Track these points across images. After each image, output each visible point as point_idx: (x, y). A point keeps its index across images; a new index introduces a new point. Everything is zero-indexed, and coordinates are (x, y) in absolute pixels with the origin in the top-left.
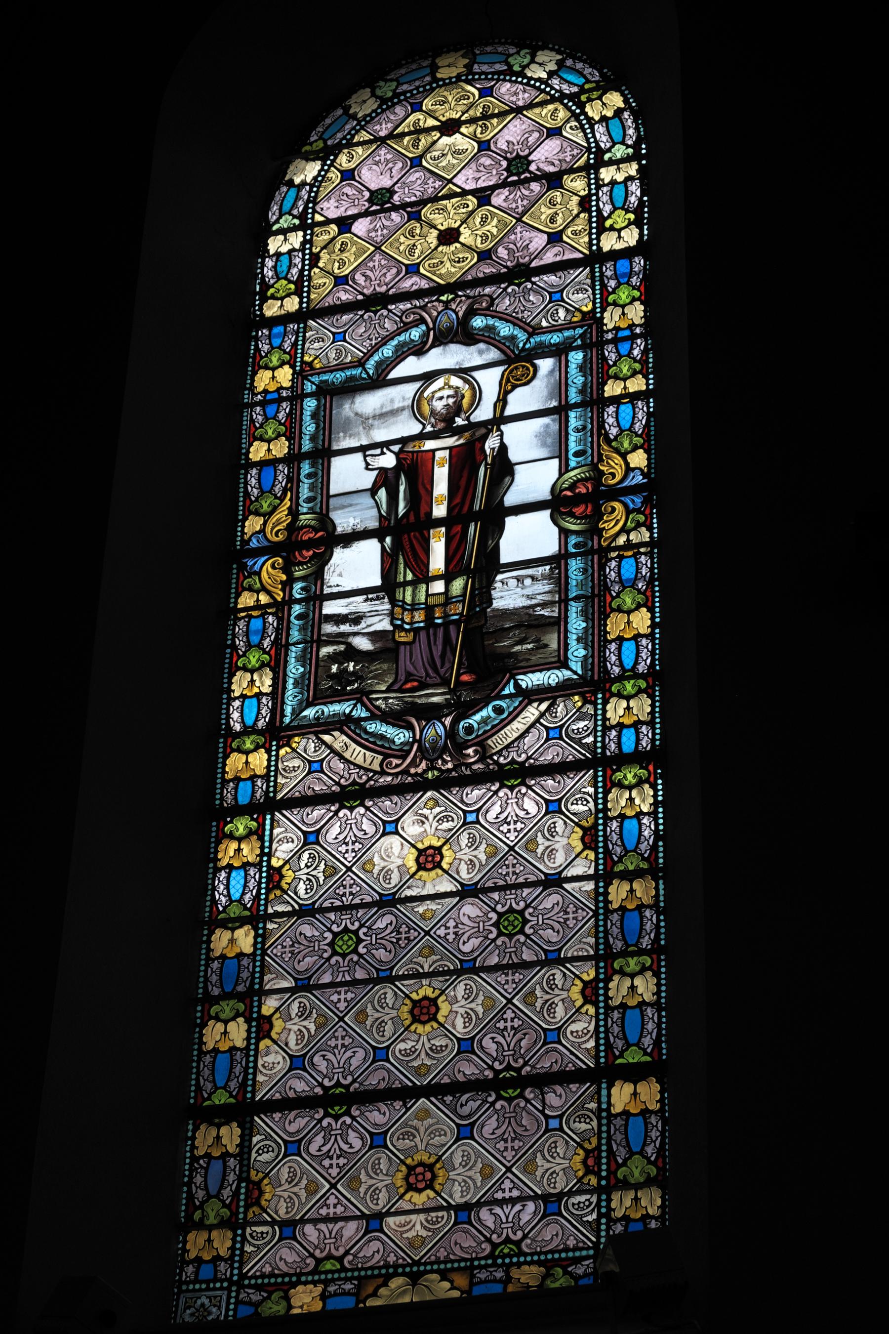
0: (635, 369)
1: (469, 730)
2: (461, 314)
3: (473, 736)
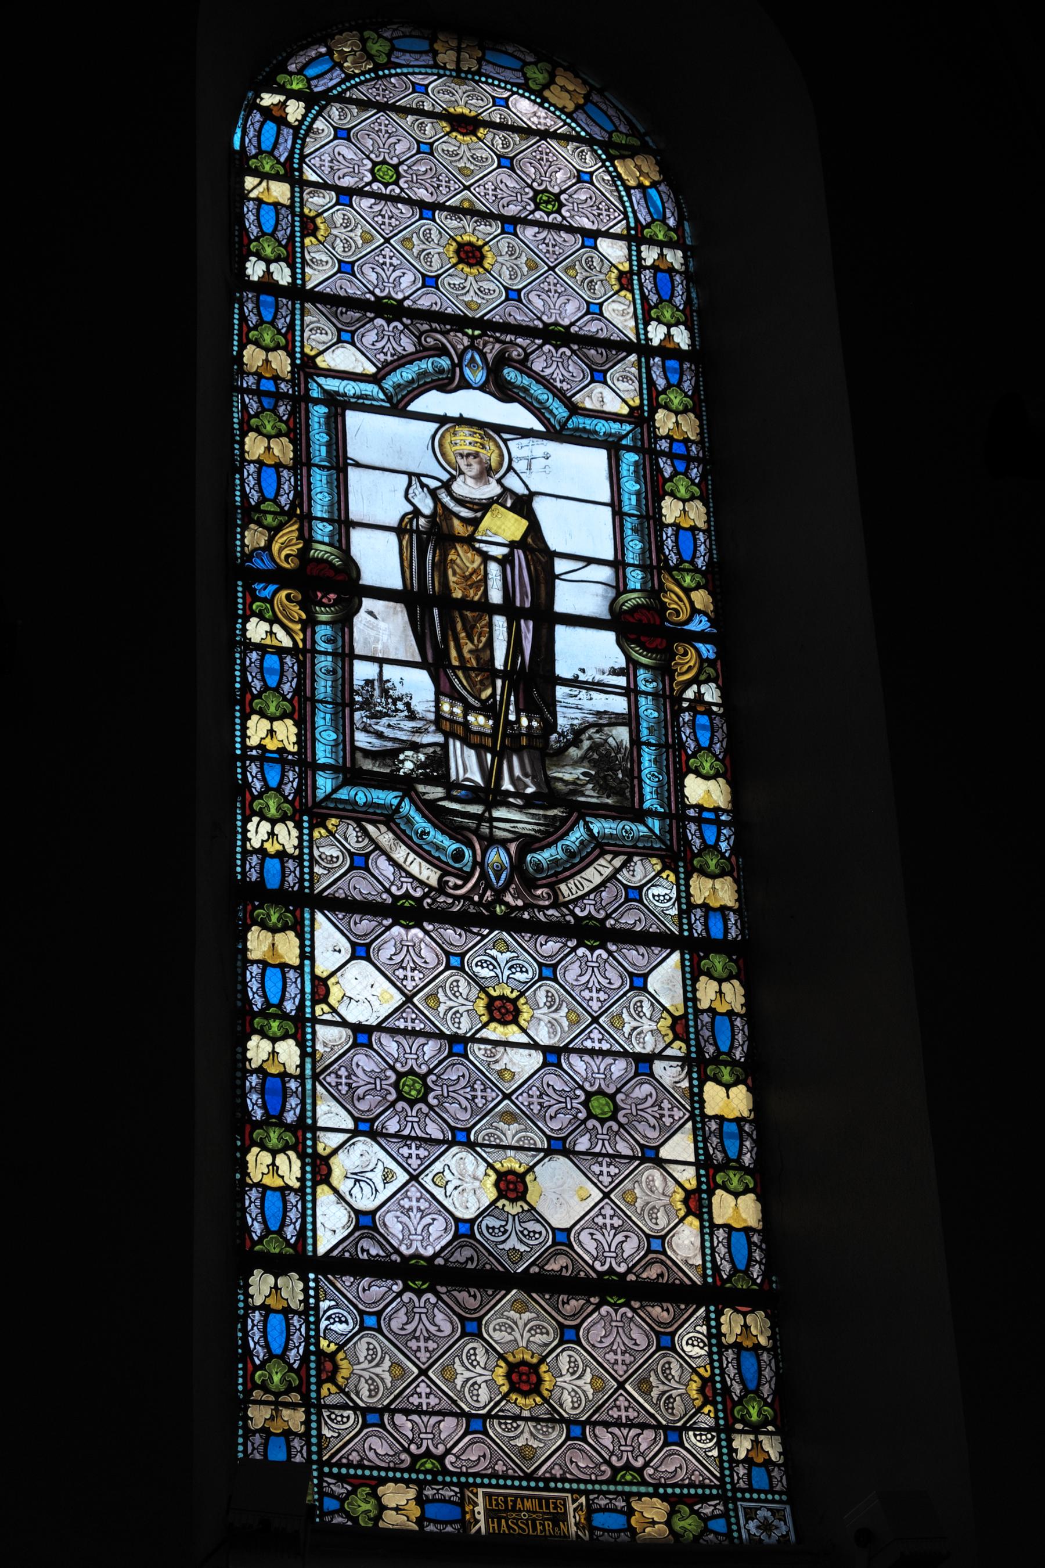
0: (280, 430)
1: (538, 867)
3: (457, 865)
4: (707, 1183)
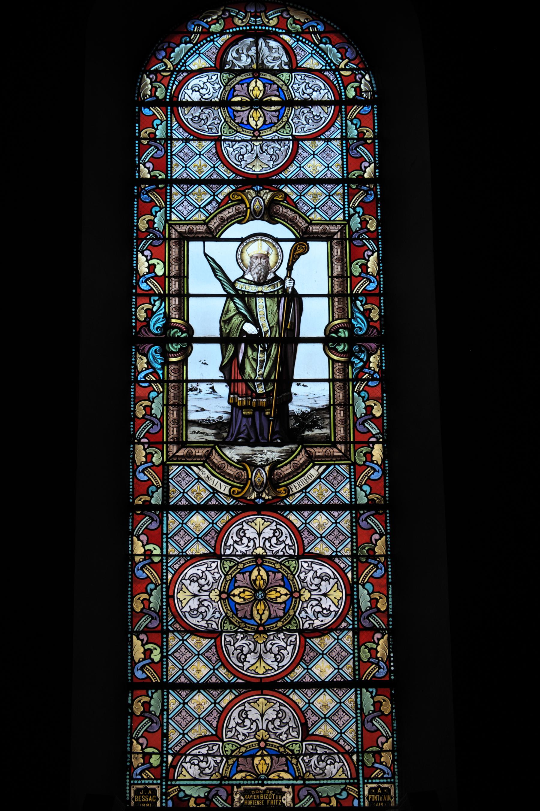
2: (266, 201)
4: (357, 612)
